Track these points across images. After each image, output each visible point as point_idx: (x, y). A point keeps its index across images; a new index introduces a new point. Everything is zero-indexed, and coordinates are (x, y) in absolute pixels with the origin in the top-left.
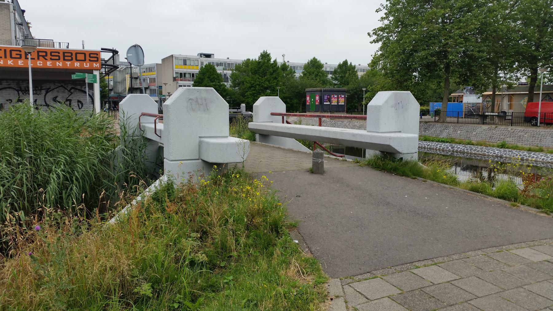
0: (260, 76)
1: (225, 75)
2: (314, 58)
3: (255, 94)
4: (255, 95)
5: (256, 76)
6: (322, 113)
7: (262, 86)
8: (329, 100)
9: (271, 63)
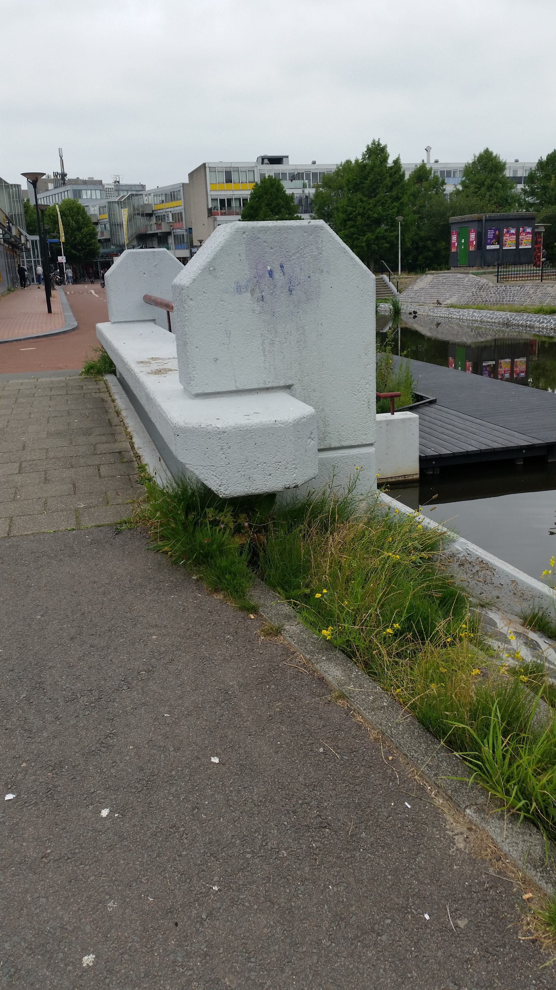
0: (365, 196)
1: (307, 197)
2: (487, 151)
3: (354, 234)
4: (355, 236)
5: (356, 196)
6: (482, 268)
7: (368, 218)
8: (499, 240)
9: (388, 166)
